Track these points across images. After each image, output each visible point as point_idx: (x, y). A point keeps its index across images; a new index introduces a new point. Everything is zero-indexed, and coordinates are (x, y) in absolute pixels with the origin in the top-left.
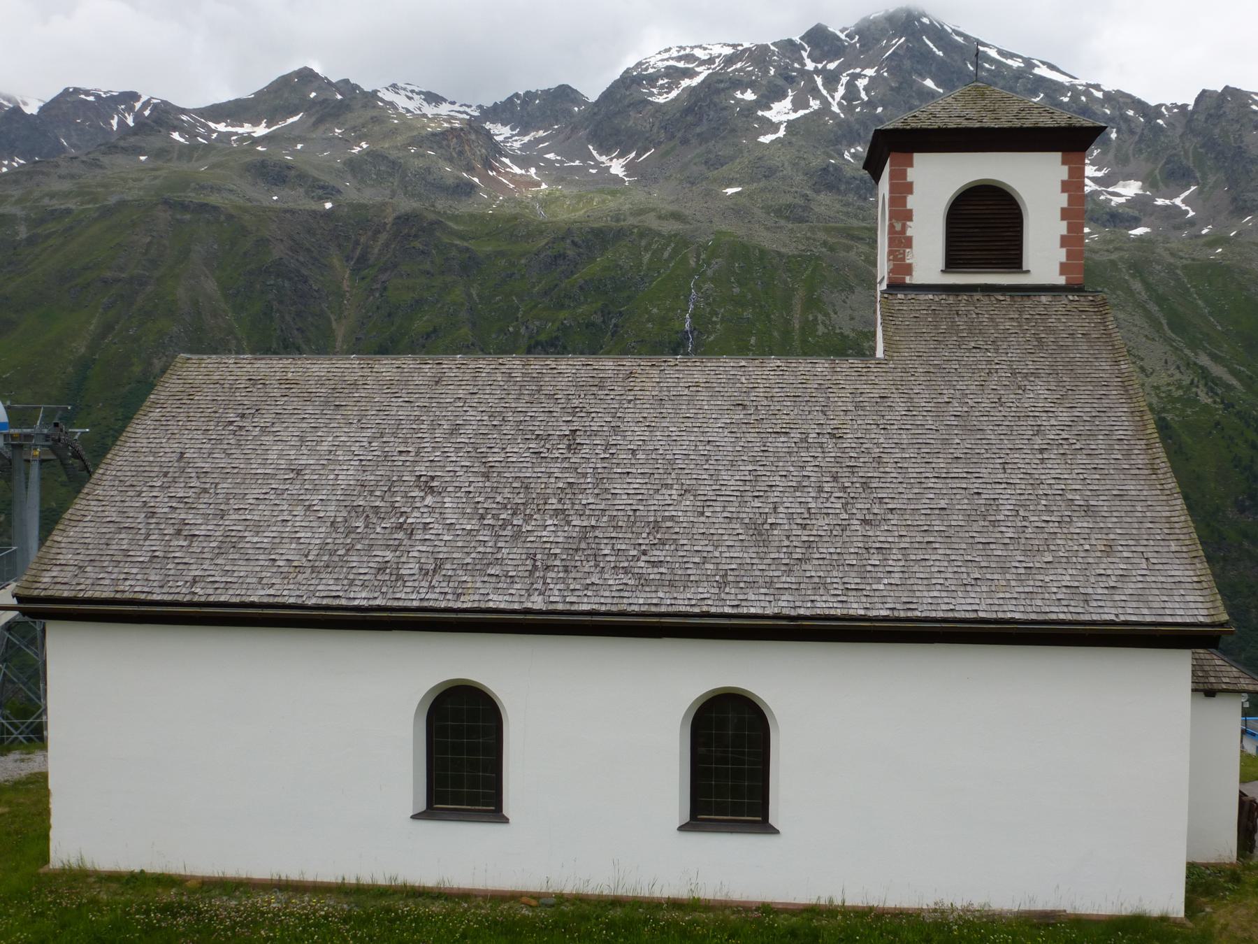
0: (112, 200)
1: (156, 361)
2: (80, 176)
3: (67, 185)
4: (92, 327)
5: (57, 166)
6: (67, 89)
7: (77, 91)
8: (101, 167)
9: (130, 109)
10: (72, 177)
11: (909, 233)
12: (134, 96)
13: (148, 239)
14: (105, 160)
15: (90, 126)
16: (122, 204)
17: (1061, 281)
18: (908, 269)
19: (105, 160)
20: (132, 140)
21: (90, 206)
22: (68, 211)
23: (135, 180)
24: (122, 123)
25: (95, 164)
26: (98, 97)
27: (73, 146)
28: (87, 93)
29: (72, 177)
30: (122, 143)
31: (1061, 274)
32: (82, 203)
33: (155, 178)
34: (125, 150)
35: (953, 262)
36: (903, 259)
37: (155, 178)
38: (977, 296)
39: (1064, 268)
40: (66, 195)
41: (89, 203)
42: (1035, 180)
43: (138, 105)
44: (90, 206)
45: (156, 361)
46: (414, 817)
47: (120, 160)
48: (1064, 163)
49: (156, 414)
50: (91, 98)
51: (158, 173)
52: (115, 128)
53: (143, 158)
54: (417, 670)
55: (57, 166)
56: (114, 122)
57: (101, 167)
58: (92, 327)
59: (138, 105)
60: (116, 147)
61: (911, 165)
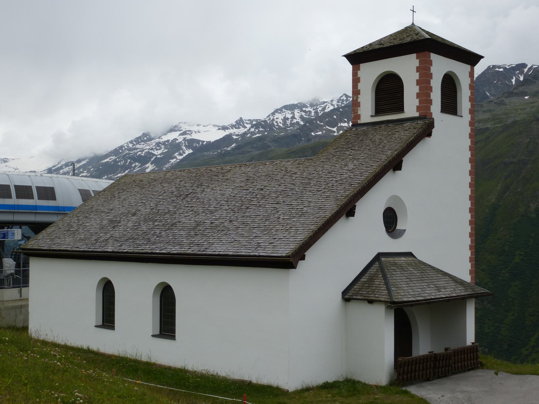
0: (509, 121)
1: (532, 205)
2: (494, 111)
3: (487, 116)
4: (498, 188)
5: (482, 106)
6: (489, 67)
7: (494, 67)
8: (504, 104)
9: (522, 73)
10: (490, 111)
11: (359, 100)
12: (524, 65)
13: (528, 140)
14: (507, 101)
15: (501, 84)
16: (515, 123)
17: (417, 114)
18: (359, 117)
19: (507, 101)
20: (521, 89)
21: (499, 125)
22: (487, 129)
23: (521, 110)
24: (517, 80)
25: (502, 103)
26: (505, 68)
27: (492, 95)
28: (499, 67)
29: (490, 111)
30: (516, 91)
31: (417, 111)
32: (495, 124)
33: (533, 107)
34: (517, 94)
35: (379, 110)
36: (357, 113)
37: (533, 107)
38: (383, 126)
39: (418, 109)
40: (487, 121)
41: (498, 124)
42: (406, 67)
43: (526, 70)
44: (499, 125)
45: (532, 205)
46: (96, 326)
47: (515, 100)
48: (417, 58)
49: (322, 214)
50: (502, 70)
51: (535, 104)
52: (514, 84)
53: (526, 97)
54: (93, 273)
55: (482, 106)
56: (513, 81)
57: (504, 104)
58: (498, 188)
59: (526, 70)
60: (512, 93)
61: (359, 70)
